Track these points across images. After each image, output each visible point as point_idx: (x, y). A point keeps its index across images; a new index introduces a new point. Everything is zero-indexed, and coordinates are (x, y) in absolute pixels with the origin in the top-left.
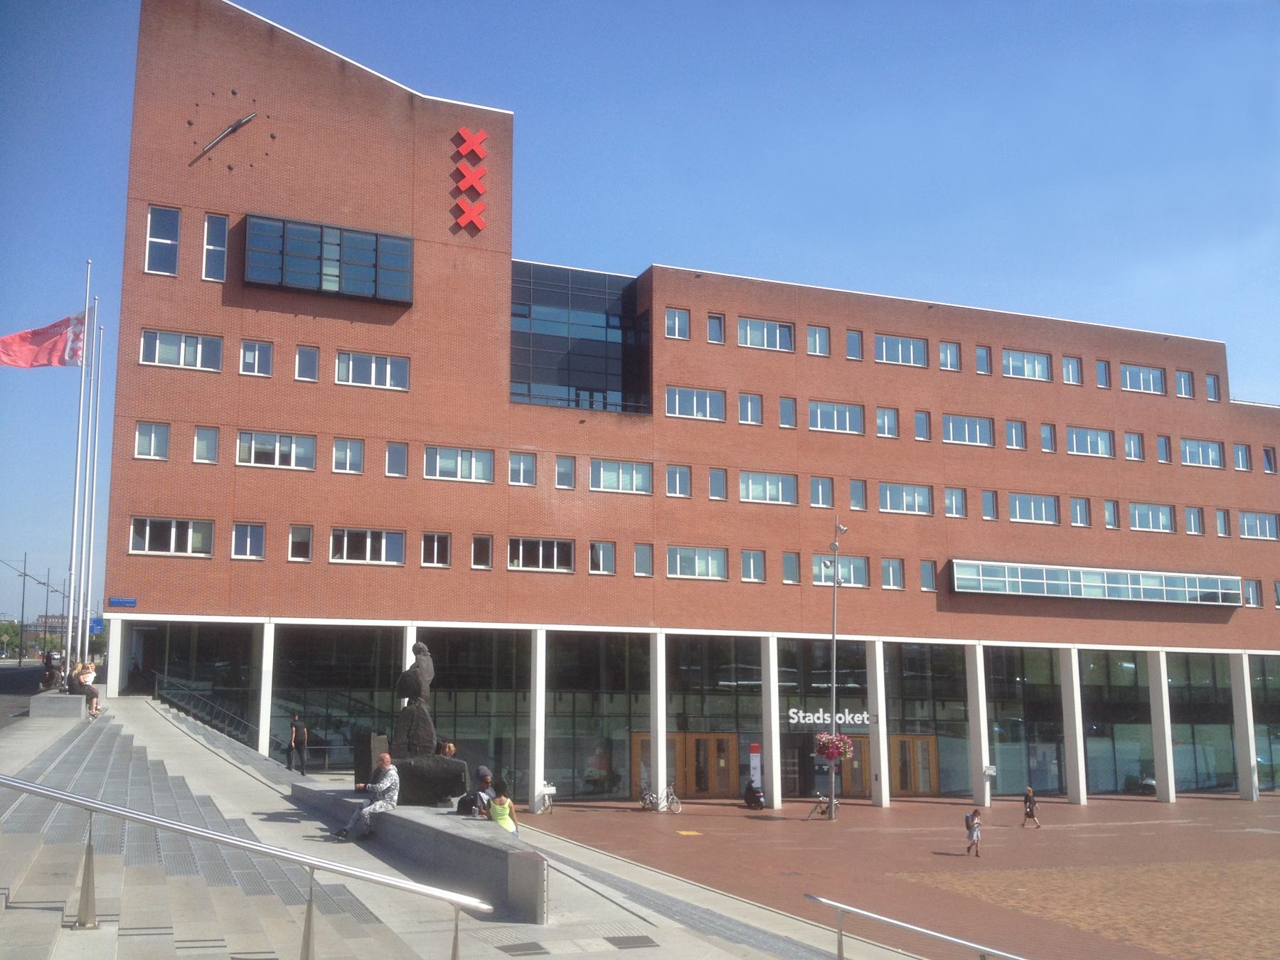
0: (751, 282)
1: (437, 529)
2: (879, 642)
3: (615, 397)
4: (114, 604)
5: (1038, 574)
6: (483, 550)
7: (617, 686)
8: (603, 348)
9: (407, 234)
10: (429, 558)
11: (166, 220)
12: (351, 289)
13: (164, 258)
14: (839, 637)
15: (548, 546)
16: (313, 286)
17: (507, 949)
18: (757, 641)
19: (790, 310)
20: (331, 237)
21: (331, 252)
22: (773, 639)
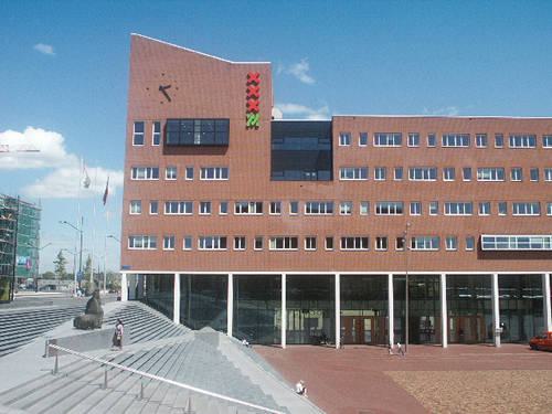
0: (509, 120)
1: (240, 235)
2: (443, 275)
3: (38, 180)
4: (123, 268)
5: (506, 240)
6: (330, 242)
7: (382, 299)
8: (304, 152)
9: (227, 117)
10: (379, 247)
11: (140, 126)
12: (205, 142)
13: (139, 140)
14: (409, 273)
15: (287, 239)
16: (189, 142)
17: (23, 408)
18: (490, 276)
19: (392, 132)
20: (198, 123)
21: (197, 129)
22: (337, 275)
